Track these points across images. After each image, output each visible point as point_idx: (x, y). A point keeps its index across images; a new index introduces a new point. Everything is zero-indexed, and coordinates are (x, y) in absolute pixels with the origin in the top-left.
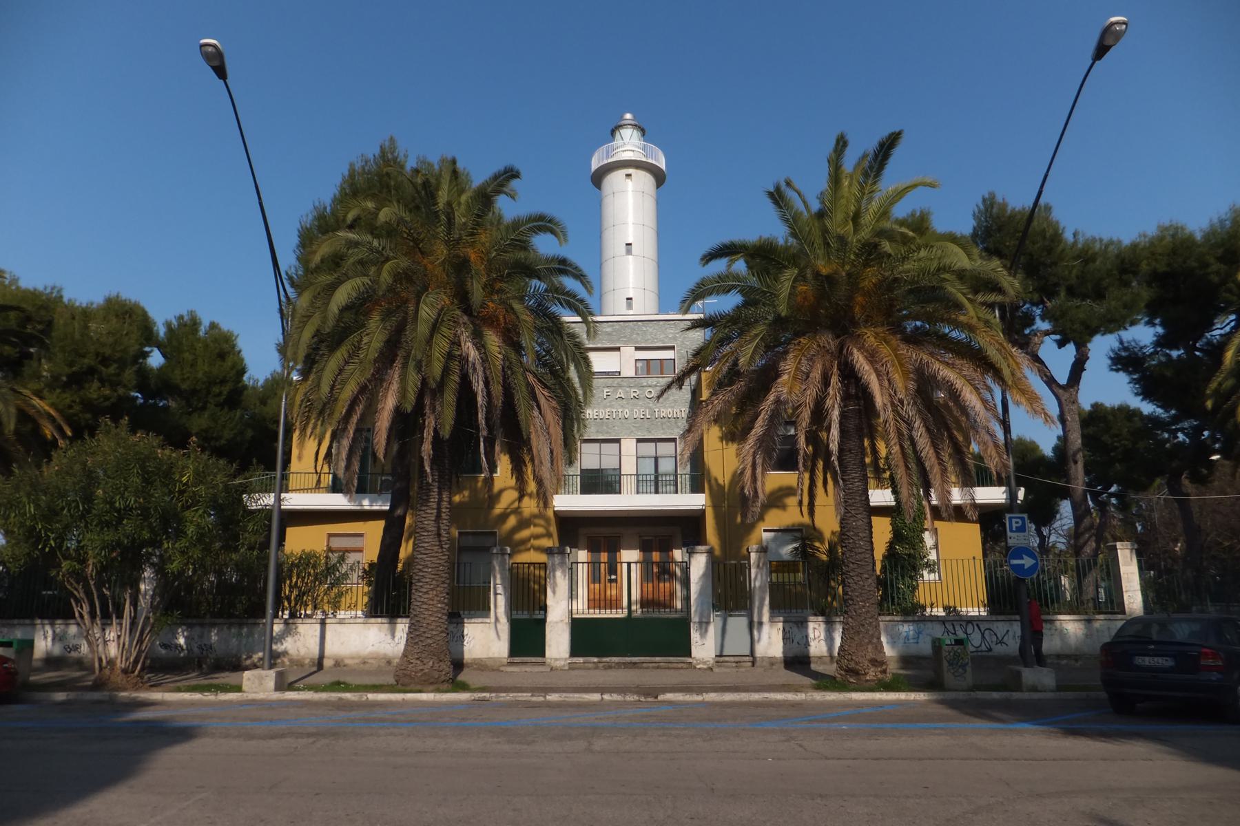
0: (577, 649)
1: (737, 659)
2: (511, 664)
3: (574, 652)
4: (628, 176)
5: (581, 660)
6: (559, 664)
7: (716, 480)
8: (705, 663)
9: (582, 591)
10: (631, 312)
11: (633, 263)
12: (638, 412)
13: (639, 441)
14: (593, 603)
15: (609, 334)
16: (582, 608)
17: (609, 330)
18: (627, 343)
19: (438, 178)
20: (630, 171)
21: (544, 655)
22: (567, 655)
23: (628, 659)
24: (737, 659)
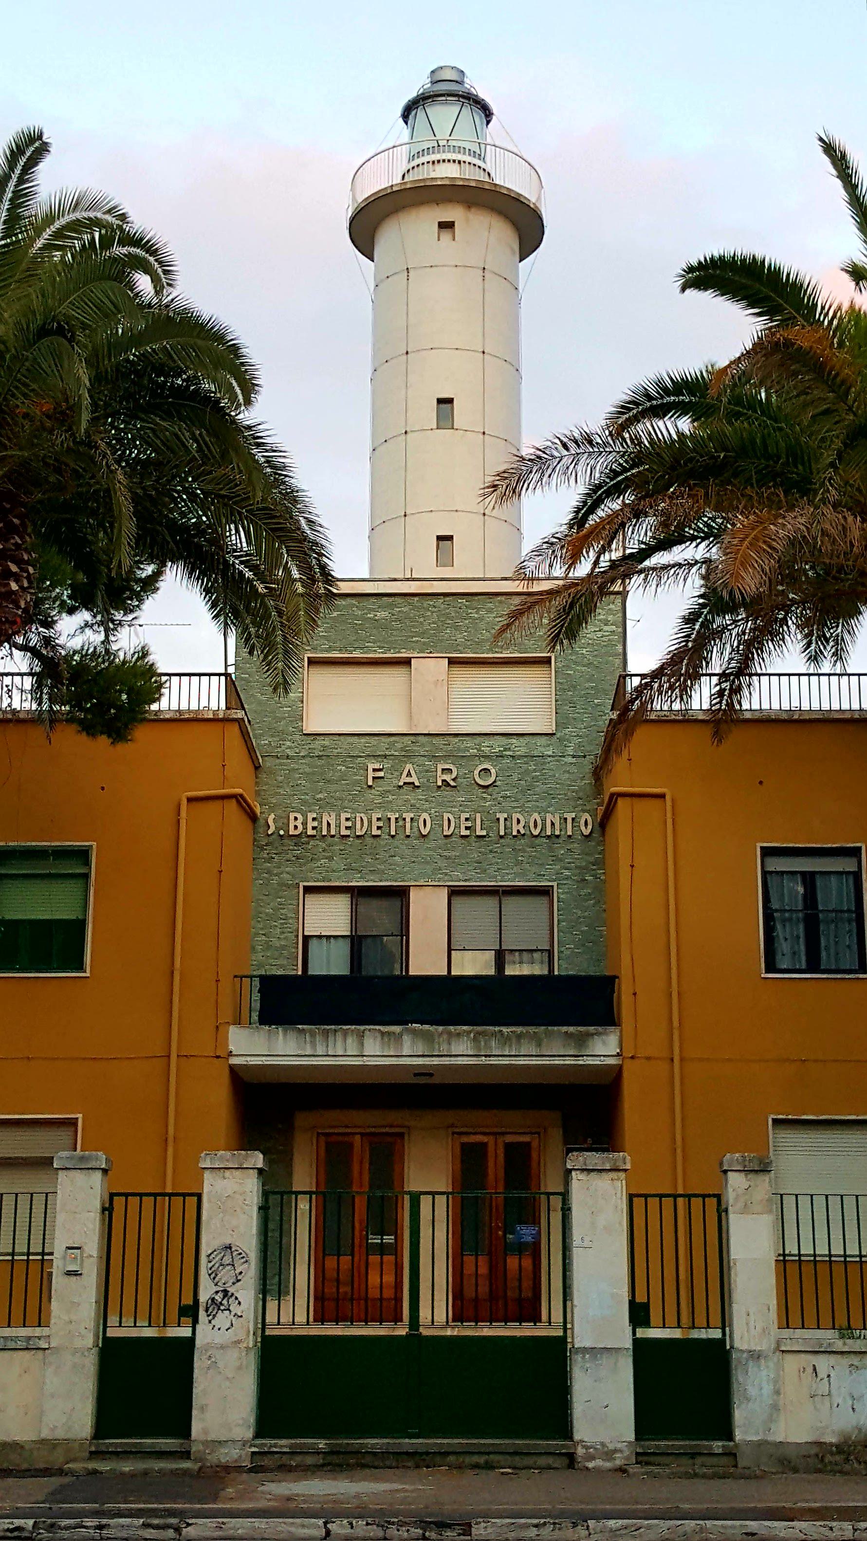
0: (271, 1417)
1: (431, 655)
2: (95, 1455)
3: (267, 1424)
4: (446, 226)
5: (284, 1444)
6: (230, 1455)
7: (572, 520)
8: (609, 1455)
9: (302, 1275)
10: (447, 572)
11: (604, 1049)
12: (454, 821)
13: (455, 893)
14: (324, 1310)
15: (382, 626)
16: (295, 1315)
17: (382, 614)
18: (429, 648)
19: (463, 1145)
20: (453, 213)
21: (185, 1431)
22: (249, 1434)
23: (408, 1443)
24: (431, 655)
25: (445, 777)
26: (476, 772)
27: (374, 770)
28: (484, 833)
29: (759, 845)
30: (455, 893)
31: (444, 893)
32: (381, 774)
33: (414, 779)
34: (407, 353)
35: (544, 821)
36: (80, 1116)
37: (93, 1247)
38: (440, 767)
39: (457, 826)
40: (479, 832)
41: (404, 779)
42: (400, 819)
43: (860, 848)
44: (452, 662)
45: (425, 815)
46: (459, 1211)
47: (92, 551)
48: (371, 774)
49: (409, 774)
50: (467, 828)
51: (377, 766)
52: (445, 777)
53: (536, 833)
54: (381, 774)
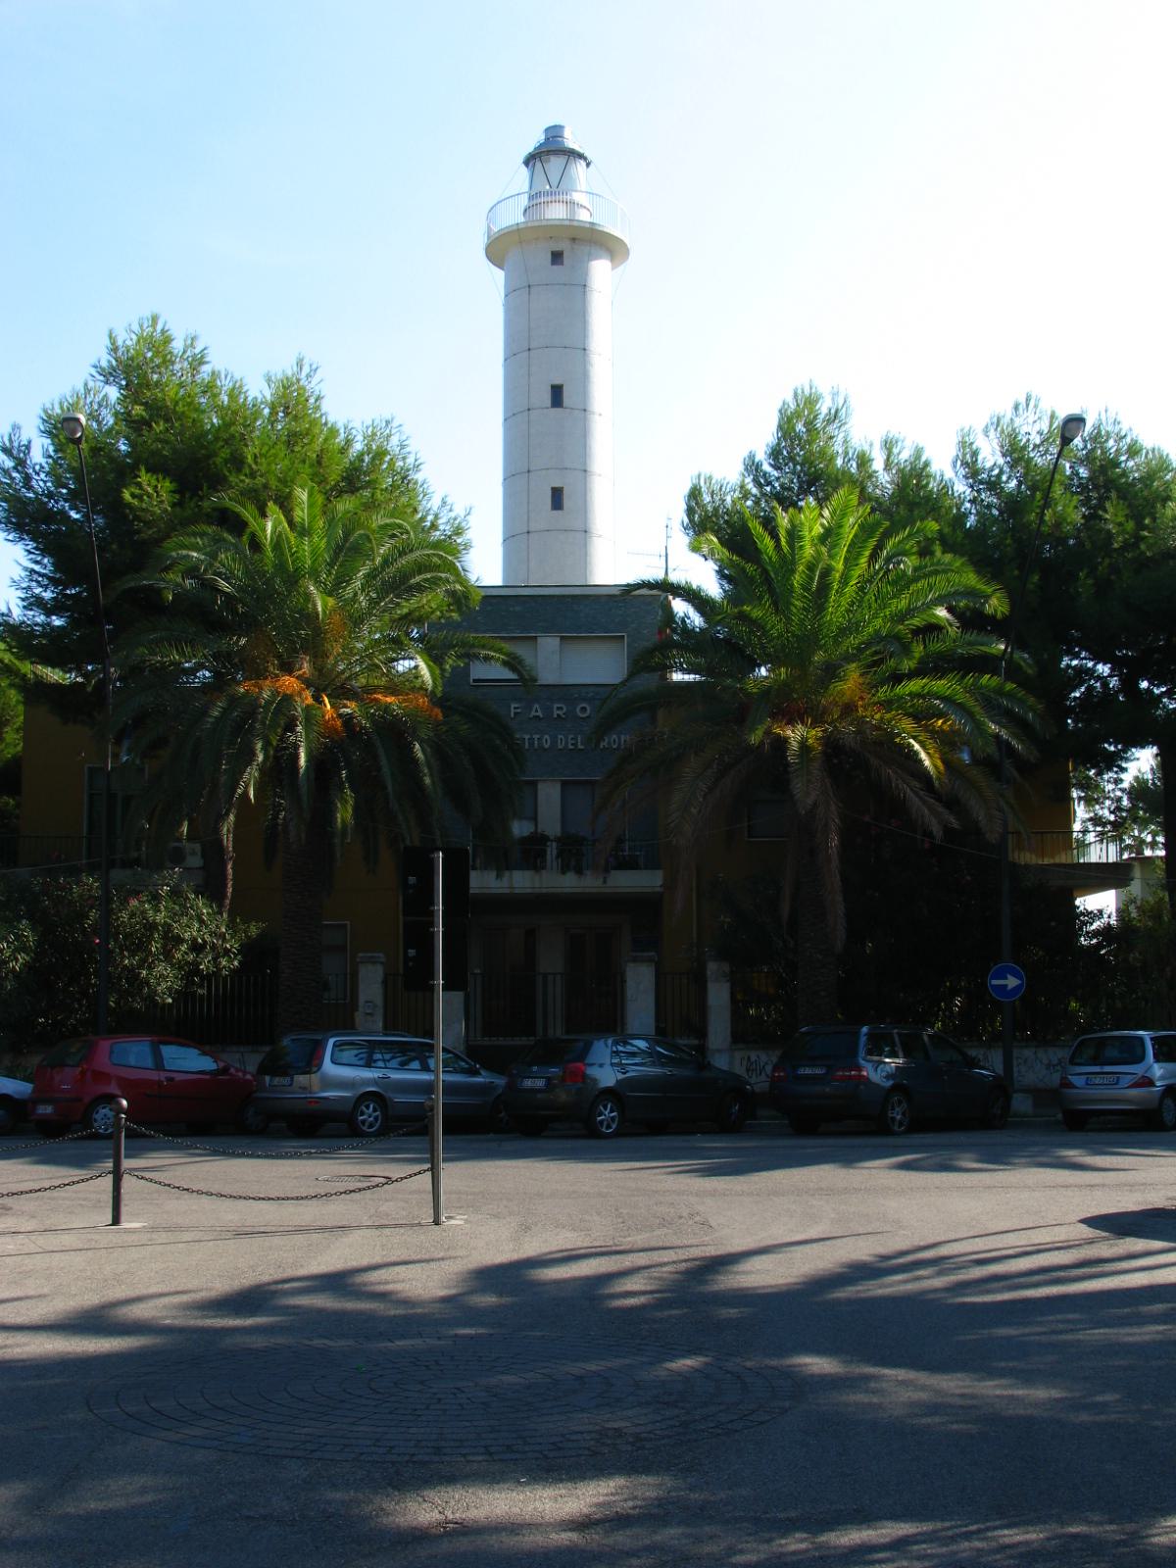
25: (558, 712)
26: (578, 710)
27: (515, 708)
28: (582, 747)
29: (87, 765)
30: (564, 784)
31: (558, 787)
32: (519, 711)
33: (539, 714)
34: (529, 471)
35: (619, 739)
36: (348, 923)
37: (379, 1001)
38: (555, 706)
39: (567, 743)
40: (581, 747)
41: (533, 713)
42: (531, 740)
43: (346, 925)
44: (562, 638)
45: (547, 737)
46: (436, 1145)
47: (74, 498)
48: (513, 711)
49: (536, 711)
50: (572, 744)
51: (516, 706)
52: (558, 712)
53: (615, 747)
54: (519, 711)
